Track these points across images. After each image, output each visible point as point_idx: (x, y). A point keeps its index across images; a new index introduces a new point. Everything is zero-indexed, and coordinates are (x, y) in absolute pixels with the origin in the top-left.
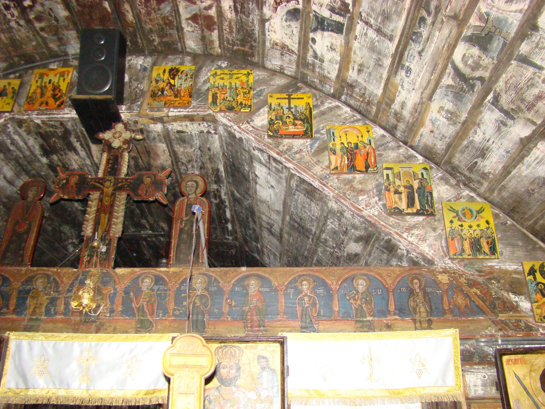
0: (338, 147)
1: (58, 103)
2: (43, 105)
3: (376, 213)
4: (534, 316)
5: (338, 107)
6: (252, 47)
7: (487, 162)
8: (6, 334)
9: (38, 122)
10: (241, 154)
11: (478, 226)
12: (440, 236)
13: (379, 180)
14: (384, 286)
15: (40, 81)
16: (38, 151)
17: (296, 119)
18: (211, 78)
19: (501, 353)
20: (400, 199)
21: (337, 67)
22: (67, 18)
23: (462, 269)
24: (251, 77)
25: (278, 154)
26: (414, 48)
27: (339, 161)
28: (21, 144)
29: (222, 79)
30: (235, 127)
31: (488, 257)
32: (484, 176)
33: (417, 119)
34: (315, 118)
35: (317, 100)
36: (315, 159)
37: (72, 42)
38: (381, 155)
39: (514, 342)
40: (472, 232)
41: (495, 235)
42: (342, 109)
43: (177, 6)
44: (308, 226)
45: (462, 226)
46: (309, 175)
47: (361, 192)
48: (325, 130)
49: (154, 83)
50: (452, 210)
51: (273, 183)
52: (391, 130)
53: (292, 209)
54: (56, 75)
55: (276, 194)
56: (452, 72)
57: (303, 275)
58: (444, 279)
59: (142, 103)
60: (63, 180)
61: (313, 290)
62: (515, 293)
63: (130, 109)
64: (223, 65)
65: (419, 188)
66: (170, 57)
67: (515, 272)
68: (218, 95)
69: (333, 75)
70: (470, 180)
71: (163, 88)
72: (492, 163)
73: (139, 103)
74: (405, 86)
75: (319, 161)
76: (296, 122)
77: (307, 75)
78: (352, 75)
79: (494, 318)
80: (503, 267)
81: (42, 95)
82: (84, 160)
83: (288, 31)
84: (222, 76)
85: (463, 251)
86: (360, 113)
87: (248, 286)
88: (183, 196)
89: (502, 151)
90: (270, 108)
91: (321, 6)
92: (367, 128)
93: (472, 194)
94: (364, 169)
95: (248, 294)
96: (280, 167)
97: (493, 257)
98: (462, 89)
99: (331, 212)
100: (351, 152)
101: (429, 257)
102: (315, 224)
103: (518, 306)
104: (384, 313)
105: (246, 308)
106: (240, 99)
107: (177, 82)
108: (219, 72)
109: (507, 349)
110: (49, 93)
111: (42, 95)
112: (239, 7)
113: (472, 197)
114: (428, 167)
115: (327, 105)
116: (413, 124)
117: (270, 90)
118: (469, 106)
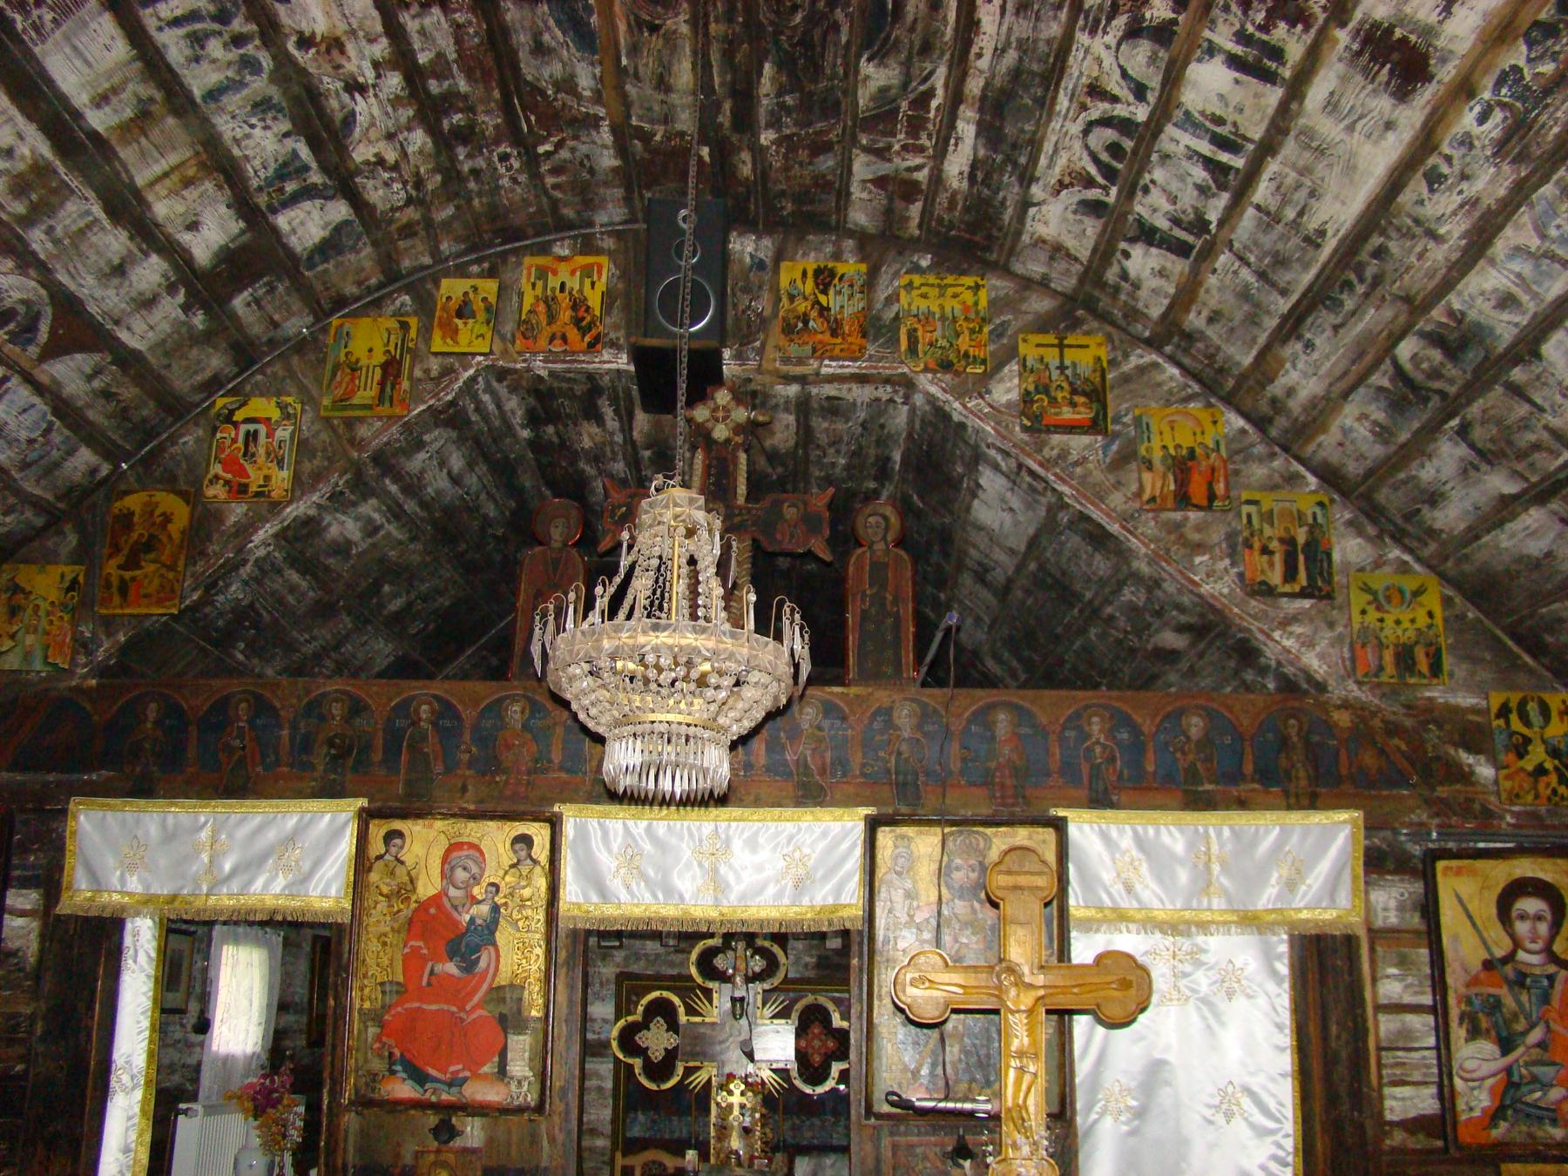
0: (1157, 455)
1: (587, 339)
2: (558, 342)
3: (1226, 591)
4: (1498, 794)
5: (1155, 365)
6: (989, 237)
7: (1436, 514)
8: (556, 809)
9: (544, 373)
10: (955, 445)
11: (1413, 621)
12: (1340, 639)
13: (1234, 524)
14: (1235, 728)
15: (540, 284)
16: (518, 419)
17: (1074, 392)
18: (903, 293)
19: (1433, 856)
20: (1271, 565)
21: (1166, 302)
22: (615, 170)
23: (1376, 701)
24: (983, 294)
25: (1041, 465)
26: (1327, 318)
27: (1159, 485)
28: (491, 407)
29: (924, 296)
30: (957, 405)
31: (1425, 681)
32: (1432, 533)
33: (1314, 420)
34: (1112, 388)
35: (1114, 348)
36: (1112, 478)
37: (610, 206)
38: (1237, 472)
39: (1460, 837)
40: (1400, 632)
41: (1441, 639)
42: (1163, 371)
43: (850, 160)
44: (1078, 587)
45: (1381, 620)
46: (1101, 510)
47: (1199, 548)
48: (1130, 416)
49: (785, 300)
50: (1366, 589)
51: (1015, 503)
52: (1261, 423)
53: (1048, 554)
54: (573, 273)
55: (1017, 523)
56: (1391, 370)
57: (1094, 705)
58: (1343, 719)
59: (763, 345)
60: (620, 507)
61: (1110, 734)
62: (1470, 749)
63: (739, 357)
64: (925, 263)
65: (1307, 544)
66: (811, 237)
67: (1474, 710)
68: (920, 333)
69: (1155, 312)
70: (1404, 533)
71: (805, 314)
72: (1451, 516)
73: (758, 344)
74: (1300, 365)
75: (1119, 483)
76: (1076, 398)
77: (1099, 300)
78: (1195, 320)
79: (1426, 793)
80: (1452, 701)
81: (552, 318)
82: (612, 434)
83: (1077, 229)
84: (924, 290)
85: (1381, 668)
86: (1199, 381)
87: (995, 723)
88: (861, 545)
89: (1467, 505)
90: (1025, 366)
91: (1155, 210)
92: (1213, 415)
93: (1407, 557)
94: (1205, 503)
95: (993, 738)
96: (1040, 486)
97: (1435, 681)
98: (1405, 398)
99: (1136, 577)
100: (1182, 465)
101: (1318, 677)
102: (1094, 587)
103: (1472, 773)
104: (1235, 777)
105: (993, 765)
106: (964, 343)
107: (832, 300)
108: (917, 280)
109: (1445, 850)
110: (566, 315)
111: (552, 318)
112: (980, 176)
113: (1406, 563)
114: (1326, 501)
115: (1134, 361)
116: (1305, 425)
117: (1020, 323)
118: (1416, 425)
